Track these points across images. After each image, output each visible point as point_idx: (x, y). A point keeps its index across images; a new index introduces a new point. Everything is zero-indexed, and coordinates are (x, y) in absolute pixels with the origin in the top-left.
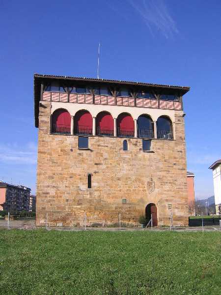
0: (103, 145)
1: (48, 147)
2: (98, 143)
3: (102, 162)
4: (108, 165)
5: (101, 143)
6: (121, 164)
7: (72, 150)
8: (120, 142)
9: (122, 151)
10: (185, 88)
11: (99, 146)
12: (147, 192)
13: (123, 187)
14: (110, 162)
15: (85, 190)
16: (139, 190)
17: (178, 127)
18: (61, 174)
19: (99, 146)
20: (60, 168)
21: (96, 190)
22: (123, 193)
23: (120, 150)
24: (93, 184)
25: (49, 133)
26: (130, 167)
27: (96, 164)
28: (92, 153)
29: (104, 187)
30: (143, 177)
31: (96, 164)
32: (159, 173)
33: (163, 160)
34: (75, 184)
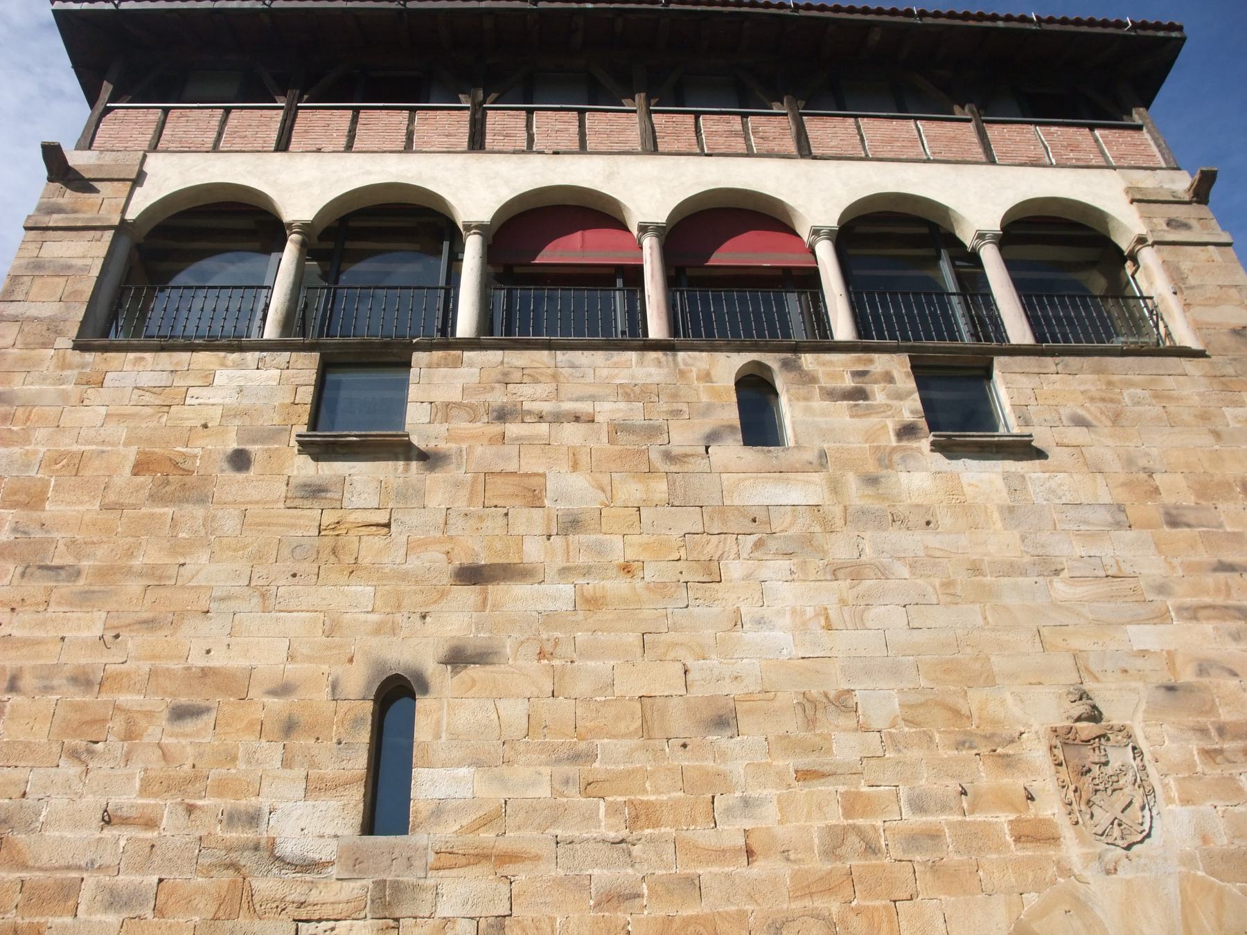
0: (546, 407)
1: (25, 439)
2: (498, 397)
3: (533, 551)
4: (593, 585)
5: (532, 396)
6: (734, 569)
7: (240, 460)
8: (707, 377)
9: (732, 452)
10: (1144, 25)
11: (502, 415)
12: (1072, 849)
13: (784, 805)
14: (619, 549)
15: (326, 851)
16: (976, 838)
17: (1185, 266)
18: (82, 680)
19: (502, 415)
20: (89, 625)
21: (449, 859)
22: (785, 871)
23: (713, 437)
24: (1126, 812)
25: (65, 342)
26: (830, 594)
27: (472, 575)
28: (438, 475)
29: (556, 815)
30: (989, 680)
31: (472, 575)
32: (1144, 637)
33: (1152, 509)
34: (221, 788)
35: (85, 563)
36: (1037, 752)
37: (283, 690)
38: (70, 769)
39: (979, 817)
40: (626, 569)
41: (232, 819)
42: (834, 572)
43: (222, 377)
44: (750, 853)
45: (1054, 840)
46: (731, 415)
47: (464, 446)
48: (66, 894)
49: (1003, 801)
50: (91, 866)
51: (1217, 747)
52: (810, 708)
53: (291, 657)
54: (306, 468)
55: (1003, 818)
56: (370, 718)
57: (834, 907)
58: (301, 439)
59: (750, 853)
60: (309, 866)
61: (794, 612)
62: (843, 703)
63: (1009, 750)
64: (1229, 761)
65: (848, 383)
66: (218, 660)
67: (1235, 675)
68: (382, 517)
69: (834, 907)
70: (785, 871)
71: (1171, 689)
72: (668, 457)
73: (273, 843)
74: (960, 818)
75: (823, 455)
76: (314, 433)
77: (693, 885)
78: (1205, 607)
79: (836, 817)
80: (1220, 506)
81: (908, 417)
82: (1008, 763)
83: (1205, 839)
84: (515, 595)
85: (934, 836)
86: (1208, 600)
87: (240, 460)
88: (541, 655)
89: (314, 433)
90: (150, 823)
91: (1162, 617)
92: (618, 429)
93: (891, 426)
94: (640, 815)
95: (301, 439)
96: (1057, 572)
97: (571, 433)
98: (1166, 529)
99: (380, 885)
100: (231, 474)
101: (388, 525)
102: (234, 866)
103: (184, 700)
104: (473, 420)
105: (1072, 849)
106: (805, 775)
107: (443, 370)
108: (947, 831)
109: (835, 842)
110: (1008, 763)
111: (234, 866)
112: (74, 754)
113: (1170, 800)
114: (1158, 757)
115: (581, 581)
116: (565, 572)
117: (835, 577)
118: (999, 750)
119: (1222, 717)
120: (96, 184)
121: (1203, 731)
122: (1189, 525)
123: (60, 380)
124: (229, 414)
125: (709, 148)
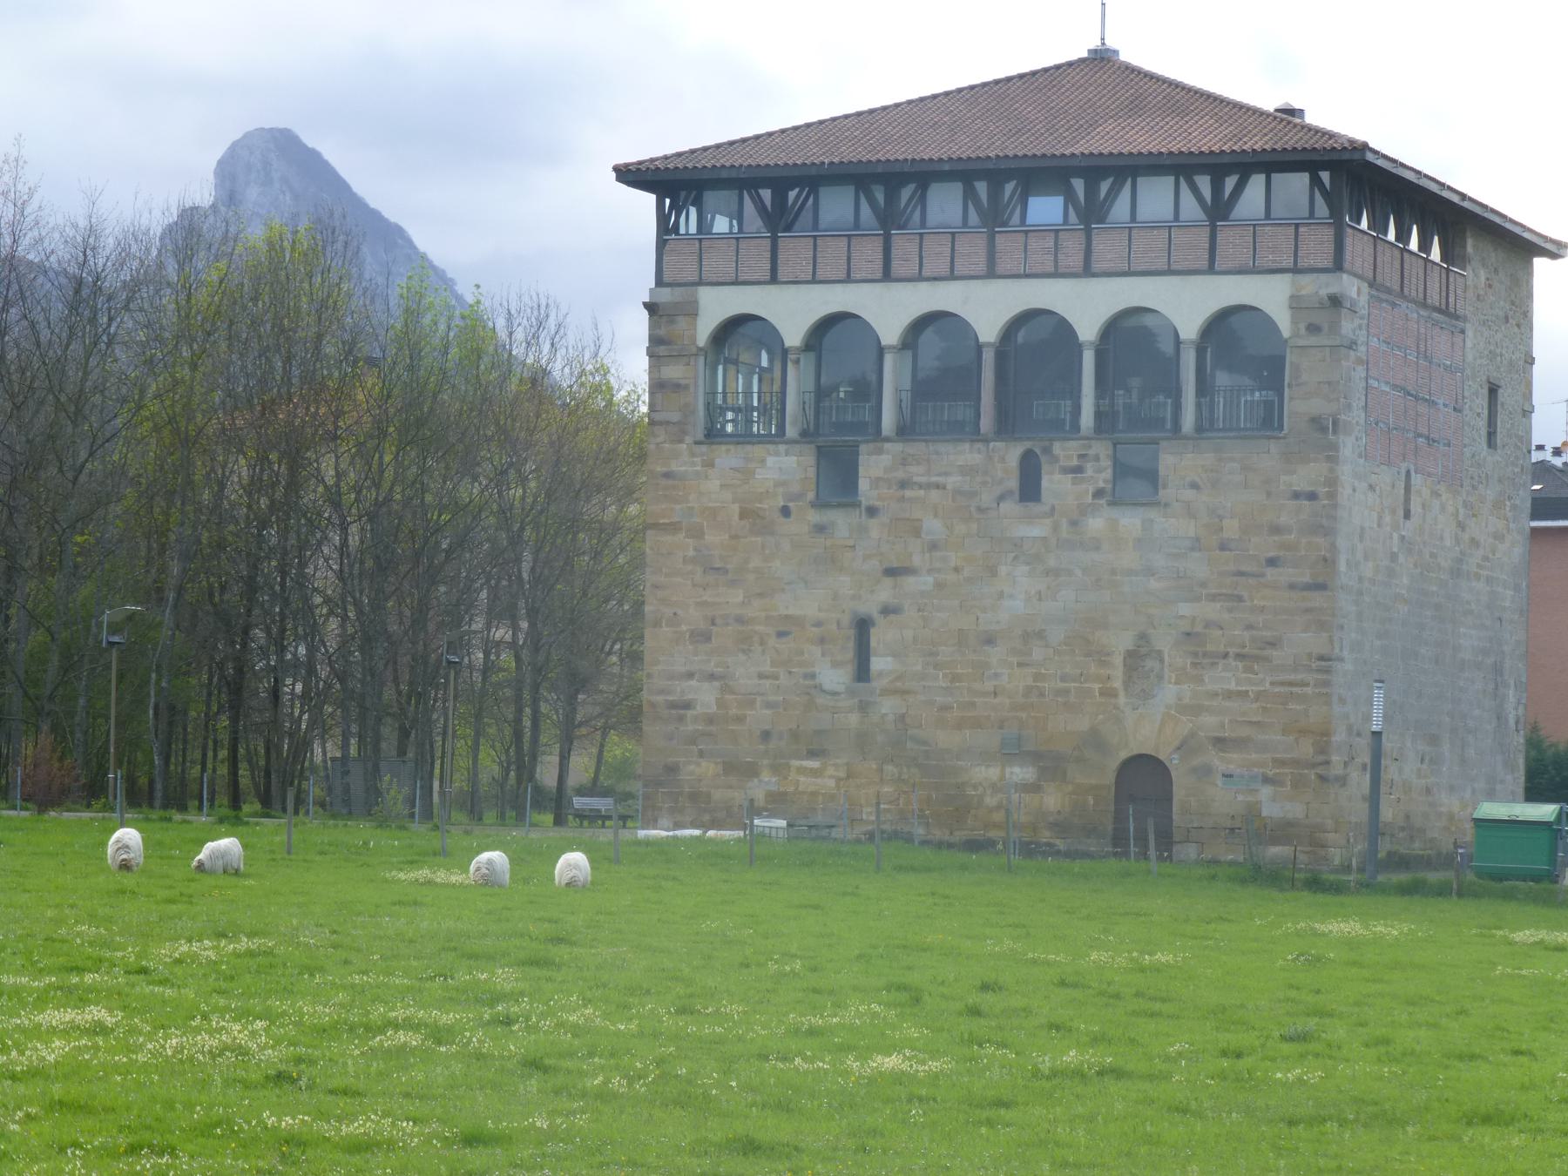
0: (923, 479)
2: (900, 474)
3: (917, 561)
5: (917, 473)
7: (786, 512)
9: (1010, 507)
11: (903, 484)
12: (1122, 700)
15: (841, 688)
19: (903, 484)
20: (737, 596)
21: (886, 692)
22: (1007, 701)
23: (1001, 498)
24: (1500, 438)
27: (891, 572)
31: (891, 572)
32: (1185, 609)
35: (728, 566)
36: (1118, 660)
37: (818, 624)
38: (742, 657)
40: (956, 570)
41: (806, 676)
42: (1047, 573)
43: (770, 461)
44: (995, 694)
45: (1116, 696)
46: (1013, 483)
47: (885, 504)
48: (752, 704)
50: (758, 694)
52: (1026, 637)
53: (820, 610)
54: (814, 516)
55: (1096, 686)
56: (853, 638)
57: (1024, 715)
58: (1017, 852)
59: (995, 694)
60: (835, 694)
61: (1026, 592)
62: (1040, 635)
65: (1075, 462)
66: (791, 612)
67: (1222, 629)
68: (851, 543)
69: (1024, 715)
70: (1007, 701)
71: (1188, 634)
72: (980, 509)
73: (821, 685)
75: (1053, 509)
77: (973, 704)
78: (1220, 595)
79: (1030, 681)
80: (1252, 540)
81: (1101, 484)
82: (1103, 664)
83: (1180, 699)
84: (910, 582)
85: (1067, 692)
86: (1224, 591)
87: (786, 512)
88: (919, 610)
90: (776, 678)
91: (1198, 599)
92: (957, 492)
93: (1091, 490)
94: (955, 678)
95: (1017, 852)
96: (1153, 575)
97: (934, 495)
98: (1217, 552)
99: (861, 701)
100: (783, 520)
101: (854, 546)
102: (808, 694)
103: (781, 629)
104: (889, 489)
105: (1122, 700)
106: (1020, 665)
107: (874, 457)
109: (1028, 691)
110: (1103, 664)
111: (808, 694)
112: (744, 651)
113: (1170, 683)
115: (936, 576)
116: (930, 571)
117: (1047, 576)
121: (1195, 654)
122: (1230, 550)
123: (694, 464)
124: (778, 484)
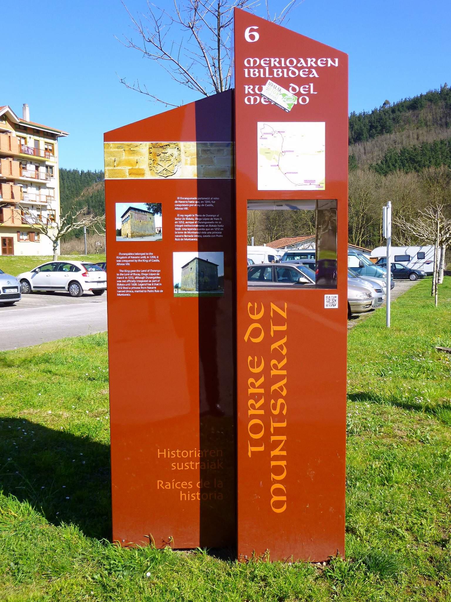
39: (119, 168)
49: (129, 163)
51: (209, 149)
63: (135, 149)
64: (211, 153)
74: (112, 168)
76: (357, 247)
89: (357, 247)
108: (107, 172)
113: (186, 164)
114: (186, 151)
118: (132, 149)
119: (389, 176)
120: (92, 293)
125: (203, 18)
